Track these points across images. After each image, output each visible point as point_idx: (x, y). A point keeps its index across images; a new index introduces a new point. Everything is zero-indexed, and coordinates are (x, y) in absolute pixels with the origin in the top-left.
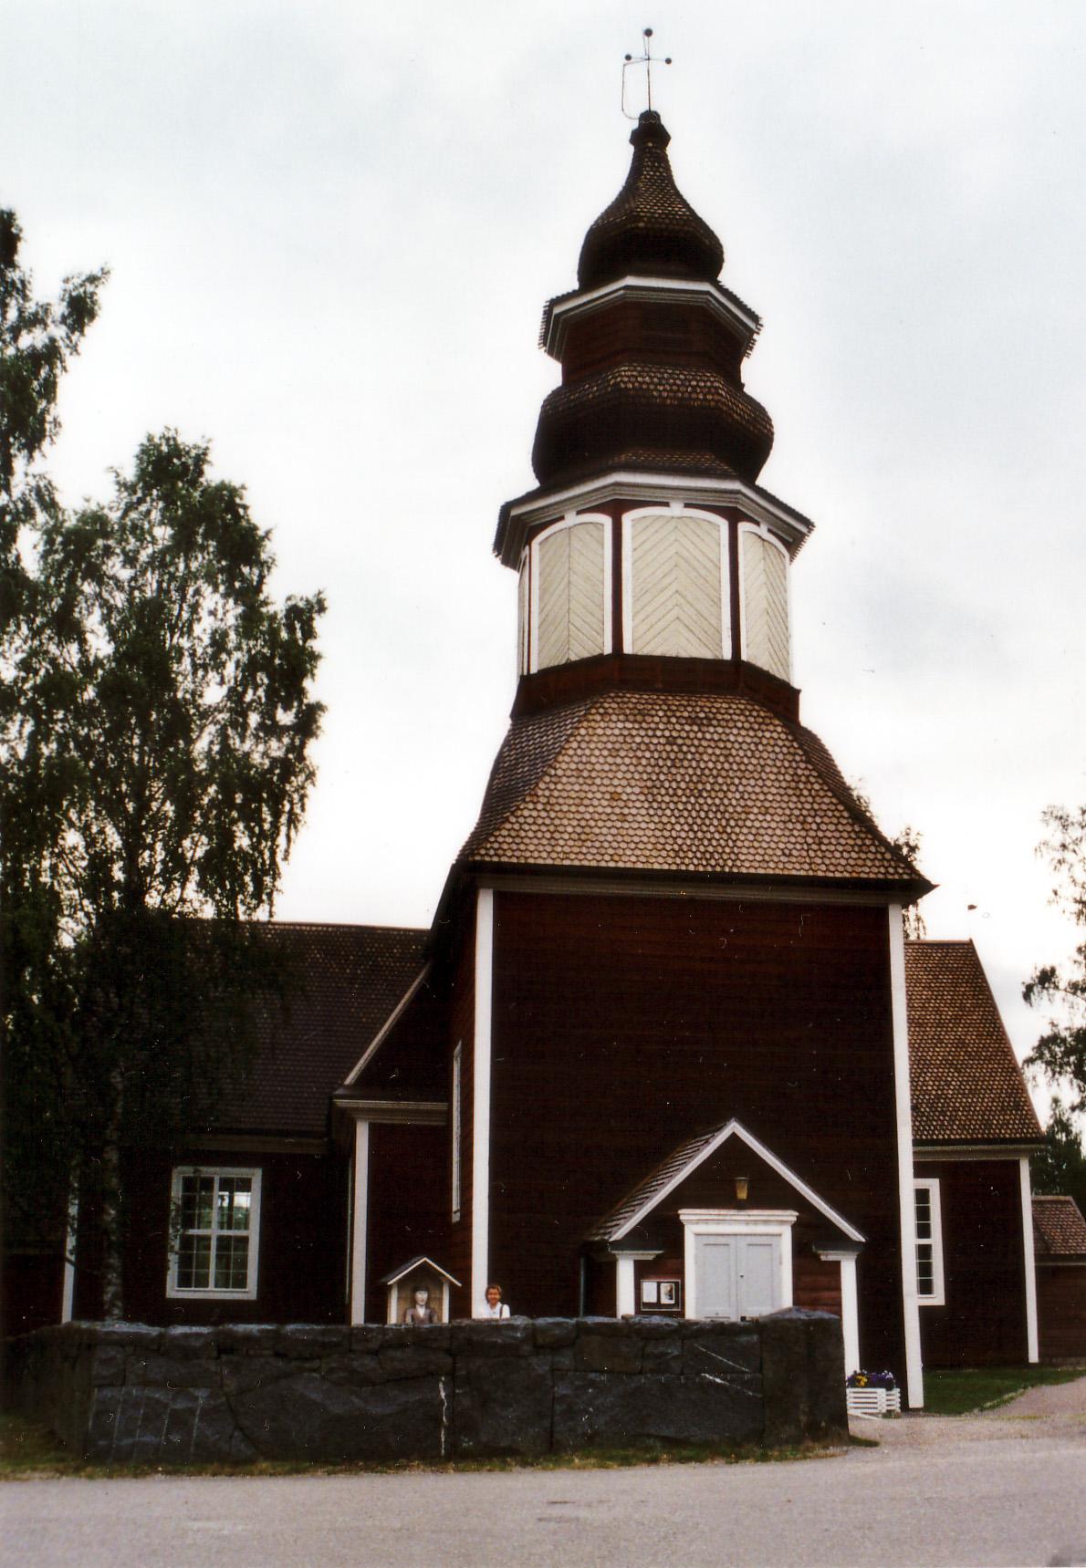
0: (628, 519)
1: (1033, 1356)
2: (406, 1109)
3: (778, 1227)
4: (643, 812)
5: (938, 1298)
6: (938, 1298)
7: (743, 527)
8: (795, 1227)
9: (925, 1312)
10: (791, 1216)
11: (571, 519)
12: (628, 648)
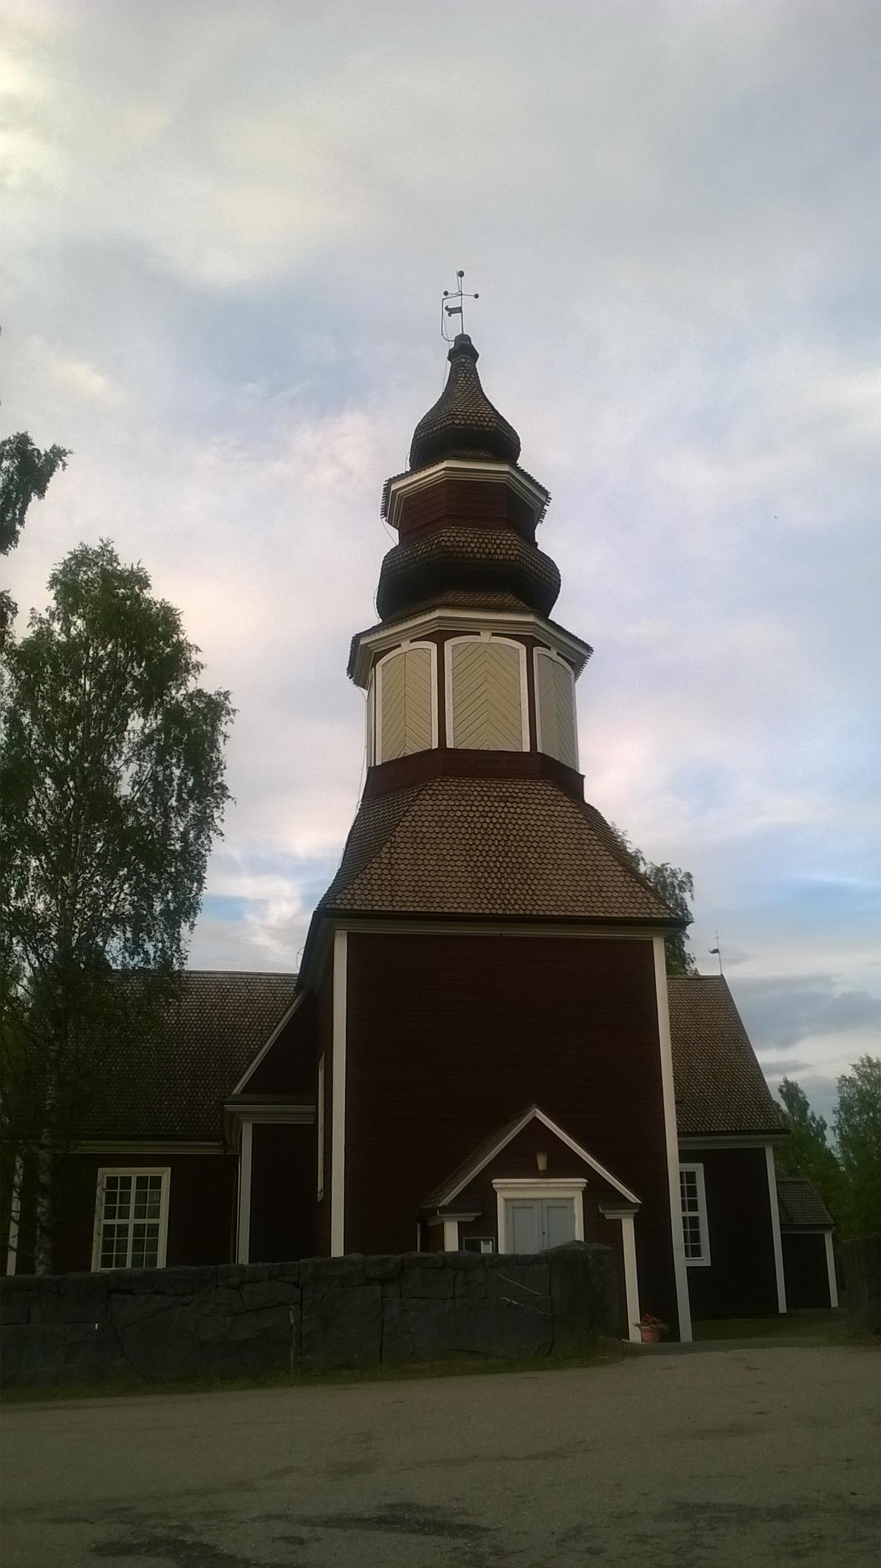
0: (448, 645)
1: (782, 1308)
2: (283, 1113)
3: (570, 1190)
4: (463, 869)
5: (705, 1260)
6: (705, 1260)
7: (537, 650)
8: (585, 1192)
9: (693, 1273)
10: (582, 1181)
11: (406, 646)
12: (450, 744)
